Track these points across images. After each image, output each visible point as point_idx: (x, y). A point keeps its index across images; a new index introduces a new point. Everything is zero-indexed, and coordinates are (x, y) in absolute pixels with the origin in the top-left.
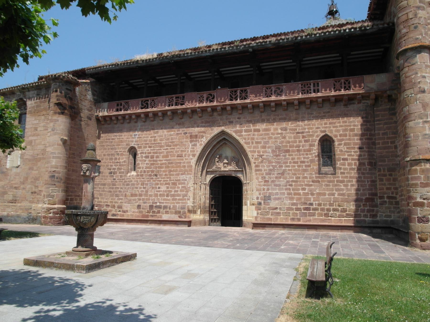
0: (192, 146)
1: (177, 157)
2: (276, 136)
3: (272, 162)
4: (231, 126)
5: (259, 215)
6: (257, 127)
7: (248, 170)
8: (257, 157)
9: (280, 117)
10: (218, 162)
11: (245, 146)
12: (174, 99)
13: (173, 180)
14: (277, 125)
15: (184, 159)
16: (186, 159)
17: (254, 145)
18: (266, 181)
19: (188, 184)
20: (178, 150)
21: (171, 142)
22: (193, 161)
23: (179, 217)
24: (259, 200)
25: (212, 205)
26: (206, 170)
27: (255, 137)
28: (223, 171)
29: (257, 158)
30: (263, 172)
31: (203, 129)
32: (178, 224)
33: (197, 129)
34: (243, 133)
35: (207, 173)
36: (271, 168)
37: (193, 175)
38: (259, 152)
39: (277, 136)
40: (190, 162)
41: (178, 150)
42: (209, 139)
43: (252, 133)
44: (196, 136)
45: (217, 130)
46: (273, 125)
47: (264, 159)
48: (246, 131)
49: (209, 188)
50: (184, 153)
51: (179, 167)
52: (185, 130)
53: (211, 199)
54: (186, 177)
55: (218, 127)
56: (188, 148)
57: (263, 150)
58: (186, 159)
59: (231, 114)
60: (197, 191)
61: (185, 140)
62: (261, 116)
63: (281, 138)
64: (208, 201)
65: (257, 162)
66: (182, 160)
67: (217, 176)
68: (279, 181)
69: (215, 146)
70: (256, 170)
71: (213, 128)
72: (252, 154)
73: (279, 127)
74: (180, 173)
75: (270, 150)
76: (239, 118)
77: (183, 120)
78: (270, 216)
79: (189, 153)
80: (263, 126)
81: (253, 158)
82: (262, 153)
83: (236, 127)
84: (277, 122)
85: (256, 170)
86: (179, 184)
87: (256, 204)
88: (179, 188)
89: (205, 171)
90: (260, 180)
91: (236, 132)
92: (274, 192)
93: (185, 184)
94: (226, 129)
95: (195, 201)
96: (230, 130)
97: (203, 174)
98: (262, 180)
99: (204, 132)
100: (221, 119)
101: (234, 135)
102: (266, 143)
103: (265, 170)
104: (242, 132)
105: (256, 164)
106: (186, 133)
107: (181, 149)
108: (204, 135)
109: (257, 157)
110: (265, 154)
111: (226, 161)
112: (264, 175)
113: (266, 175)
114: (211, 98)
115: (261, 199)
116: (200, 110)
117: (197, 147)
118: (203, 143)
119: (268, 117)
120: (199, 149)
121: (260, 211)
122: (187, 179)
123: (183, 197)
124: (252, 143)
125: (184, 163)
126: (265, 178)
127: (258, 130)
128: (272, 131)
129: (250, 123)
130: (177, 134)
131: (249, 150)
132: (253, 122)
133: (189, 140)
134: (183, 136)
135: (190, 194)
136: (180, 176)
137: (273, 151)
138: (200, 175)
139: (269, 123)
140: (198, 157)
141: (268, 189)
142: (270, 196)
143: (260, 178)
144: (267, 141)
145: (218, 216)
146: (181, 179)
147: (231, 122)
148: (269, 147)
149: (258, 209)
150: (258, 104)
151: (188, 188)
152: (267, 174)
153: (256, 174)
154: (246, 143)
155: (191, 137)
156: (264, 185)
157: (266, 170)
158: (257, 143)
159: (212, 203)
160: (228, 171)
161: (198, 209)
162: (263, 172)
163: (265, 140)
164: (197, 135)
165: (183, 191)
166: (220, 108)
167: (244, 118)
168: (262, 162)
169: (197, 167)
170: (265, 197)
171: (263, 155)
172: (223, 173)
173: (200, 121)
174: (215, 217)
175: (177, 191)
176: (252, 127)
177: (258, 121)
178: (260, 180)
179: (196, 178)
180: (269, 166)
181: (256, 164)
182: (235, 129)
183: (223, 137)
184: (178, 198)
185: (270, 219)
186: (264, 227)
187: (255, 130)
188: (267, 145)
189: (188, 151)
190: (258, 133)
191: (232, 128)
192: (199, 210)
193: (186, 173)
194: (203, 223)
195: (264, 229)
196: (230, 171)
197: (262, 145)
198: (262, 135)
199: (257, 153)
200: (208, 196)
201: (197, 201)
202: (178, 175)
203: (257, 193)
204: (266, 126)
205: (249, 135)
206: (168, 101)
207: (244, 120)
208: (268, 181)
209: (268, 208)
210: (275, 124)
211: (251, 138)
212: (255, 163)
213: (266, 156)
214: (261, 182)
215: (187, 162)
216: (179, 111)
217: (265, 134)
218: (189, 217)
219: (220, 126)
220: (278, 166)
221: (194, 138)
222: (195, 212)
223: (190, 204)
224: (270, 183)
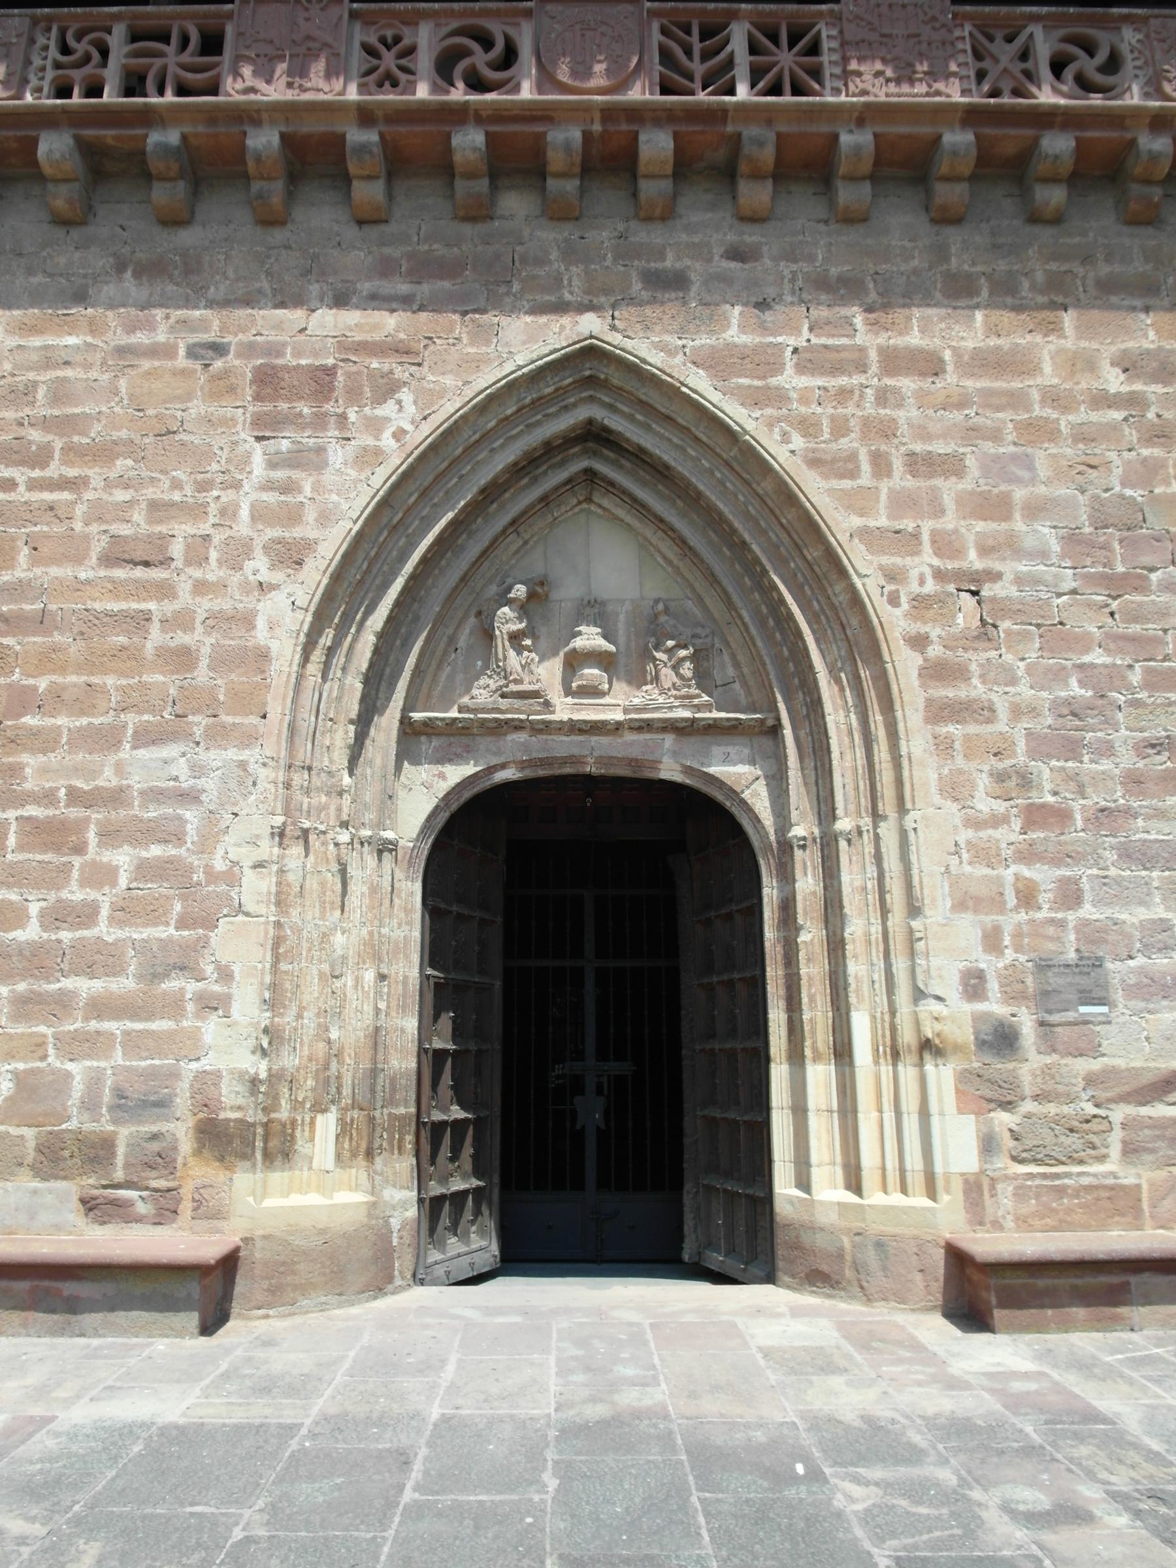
0: (272, 465)
1: (109, 560)
2: (1083, 415)
3: (1084, 643)
4: (671, 309)
5: (1002, 1164)
6: (914, 339)
7: (837, 716)
8: (930, 587)
9: (1104, 269)
10: (515, 638)
11: (817, 492)
12: (117, 40)
13: (48, 797)
14: (1083, 331)
15: (184, 588)
16: (201, 587)
17: (900, 479)
18: (1035, 816)
19: (207, 842)
20: (121, 496)
21: (45, 424)
22: (283, 612)
23: (89, 1205)
24: (995, 1006)
25: (439, 1056)
26: (405, 721)
27: (901, 415)
28: (574, 728)
29: (940, 600)
30: (1001, 726)
31: (390, 323)
32: (73, 1307)
33: (328, 322)
34: (790, 379)
35: (414, 739)
36: (1075, 689)
37: (273, 745)
38: (945, 545)
39: (1094, 416)
40: (248, 620)
41: (121, 496)
42: (448, 408)
43: (872, 379)
44: (321, 382)
45: (530, 339)
46: (1054, 328)
47: (1004, 608)
48: (808, 361)
49: (417, 887)
50: (183, 530)
51: (129, 657)
52: (210, 322)
53: (446, 992)
54: (198, 770)
55: (533, 311)
56: (237, 485)
57: (980, 526)
58: (201, 587)
59: (666, 214)
60: (306, 918)
61: (198, 407)
62: (941, 254)
63: (1131, 434)
64: (411, 1024)
65: (935, 632)
66: (165, 591)
67: (509, 774)
68: (1161, 814)
69: (490, 494)
70: (938, 712)
71: (489, 318)
72: (885, 560)
73: (1108, 350)
74: (131, 720)
75: (1046, 534)
76: (736, 254)
77: (187, 237)
78: (1112, 1167)
79: (243, 526)
80: (959, 330)
81: (894, 600)
82: (973, 560)
83: (718, 323)
84: (1078, 304)
85: (938, 712)
86: (109, 836)
87: (958, 1048)
88: (102, 875)
89: (387, 725)
90: (984, 805)
91: (718, 363)
92: (1133, 916)
93: (178, 838)
94: (616, 338)
95: (288, 1019)
96: (656, 343)
97: (369, 750)
98: (1000, 806)
99: (401, 350)
100: (570, 254)
101: (700, 384)
102: (995, 467)
103: (1017, 712)
104: (778, 368)
105: (935, 651)
106: (219, 349)
107: (150, 493)
108: (400, 373)
109: (930, 587)
110: (1010, 568)
111: (590, 638)
112: (1021, 757)
113: (1033, 754)
114: (480, 59)
115: (1013, 996)
116: (371, 137)
117: (328, 477)
118: (387, 441)
119: (1002, 266)
120: (345, 491)
121: (1003, 1119)
122: (210, 785)
123: (152, 974)
124: (881, 465)
125: (182, 621)
126: (1026, 781)
127: (931, 365)
128: (1049, 375)
129: (844, 301)
130: (121, 351)
131: (857, 521)
132: (873, 296)
133: (241, 410)
134: (183, 373)
135: (239, 947)
136: (125, 752)
137: (1072, 539)
138: (340, 758)
139: (1018, 309)
140: (337, 577)
141: (1070, 895)
142: (1098, 964)
143: (983, 782)
144: (1014, 458)
145: (478, 1171)
146: (137, 781)
147: (665, 284)
148: (1035, 510)
149: (990, 1094)
150: (925, 130)
151: (212, 876)
152: (1040, 747)
153: (944, 747)
154: (814, 462)
155: (268, 381)
156: (1028, 855)
157: (1034, 711)
158: (918, 464)
159: (438, 1044)
160: (618, 727)
161: (319, 1108)
162: (1001, 726)
163: (989, 447)
164: (330, 371)
165: (153, 914)
166: (575, 134)
167: (790, 256)
168: (986, 631)
169: (314, 668)
170: (1043, 966)
171: (994, 576)
172: (563, 746)
173: (359, 257)
174: (458, 1185)
175: (86, 915)
176: (863, 333)
177: (914, 292)
178: (984, 805)
179: (299, 778)
180: (1059, 675)
181: (935, 651)
182: (704, 340)
183: (582, 413)
184: (84, 986)
185: (1120, 1202)
186: (1116, 1296)
187: (893, 362)
188: (1019, 494)
189: (228, 513)
190: (926, 384)
191: (681, 332)
192: (327, 1124)
193: (199, 722)
194: (360, 1266)
195: (1111, 1324)
196: (645, 726)
197: (967, 485)
198: (962, 404)
199: (927, 559)
200: (415, 973)
201: (310, 1020)
202: (108, 739)
203: (967, 930)
204: (993, 330)
205: (843, 394)
206: (54, 53)
207: (786, 269)
208: (1062, 816)
209: (1091, 1080)
210: (1068, 319)
211: (866, 422)
212: (919, 642)
213: (1019, 580)
214: (997, 821)
215: (216, 621)
216: (155, 138)
217: (987, 393)
218: (209, 1212)
219: (561, 308)
220: (1135, 678)
221: (289, 395)
222: (275, 1145)
223: (226, 1052)
224: (1077, 834)
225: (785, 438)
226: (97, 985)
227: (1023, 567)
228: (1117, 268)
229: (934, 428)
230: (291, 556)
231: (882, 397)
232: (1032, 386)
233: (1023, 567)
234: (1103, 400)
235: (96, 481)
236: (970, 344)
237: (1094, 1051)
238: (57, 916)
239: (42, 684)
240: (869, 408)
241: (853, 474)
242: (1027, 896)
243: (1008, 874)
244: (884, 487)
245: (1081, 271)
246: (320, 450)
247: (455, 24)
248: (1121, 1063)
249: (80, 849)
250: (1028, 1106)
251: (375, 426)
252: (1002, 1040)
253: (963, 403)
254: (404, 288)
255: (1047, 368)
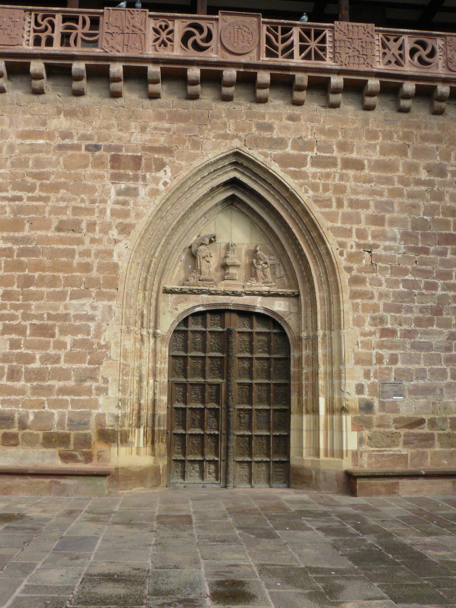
17: (346, 209)
50: (85, 219)
51: (67, 267)
70: (354, 295)
88: (61, 345)
124: (340, 204)
126: (382, 320)
152: (388, 308)
153: (355, 307)
156: (381, 346)
175: (57, 360)
180: (396, 283)
184: (57, 384)
202: (61, 296)
208: (392, 333)
238: (46, 359)
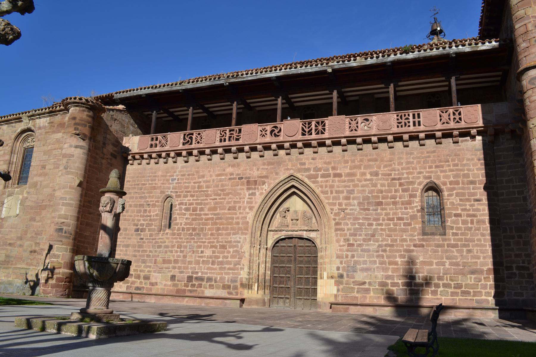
1: (229, 210)
3: (359, 219)
9: (369, 157)
12: (227, 132)
13: (222, 242)
15: (238, 213)
16: (240, 213)
17: (334, 194)
19: (241, 249)
20: (230, 200)
22: (250, 216)
24: (341, 272)
27: (335, 184)
30: (346, 232)
34: (319, 179)
38: (340, 204)
40: (246, 218)
41: (230, 200)
43: (332, 178)
51: (231, 224)
57: (345, 201)
58: (240, 213)
63: (370, 185)
65: (337, 218)
66: (236, 214)
72: (331, 207)
81: (332, 213)
82: (344, 207)
86: (230, 248)
87: (335, 277)
90: (342, 243)
98: (344, 244)
105: (337, 221)
107: (234, 200)
110: (349, 208)
118: (264, 191)
122: (241, 240)
123: (235, 265)
124: (332, 193)
131: (327, 201)
133: (245, 187)
137: (359, 204)
141: (353, 256)
143: (342, 240)
148: (354, 199)
151: (242, 252)
152: (351, 235)
153: (337, 235)
154: (322, 192)
156: (348, 251)
158: (337, 192)
163: (348, 189)
164: (256, 181)
175: (227, 257)
180: (355, 224)
181: (337, 221)
193: (240, 232)
202: (229, 234)
205: (327, 181)
207: (320, 161)
208: (353, 245)
209: (353, 282)
212: (335, 219)
213: (350, 210)
214: (343, 246)
222: (249, 287)
225: (318, 189)
226: (229, 266)
227: (351, 207)
228: (371, 157)
229: (340, 186)
230: (251, 208)
231: (333, 181)
232: (355, 178)
233: (351, 207)
234: (366, 180)
235: (227, 198)
236: (347, 172)
237: (354, 278)
238: (224, 257)
239: (221, 227)
240: (331, 183)
241: (327, 194)
242: (347, 256)
243: (344, 253)
244: (332, 196)
245: (365, 158)
246: (255, 193)
247: (273, 126)
248: (358, 280)
249: (226, 249)
250: (344, 285)
251: (262, 189)
252: (341, 276)
253: (345, 182)
254: (266, 167)
255: (358, 175)
